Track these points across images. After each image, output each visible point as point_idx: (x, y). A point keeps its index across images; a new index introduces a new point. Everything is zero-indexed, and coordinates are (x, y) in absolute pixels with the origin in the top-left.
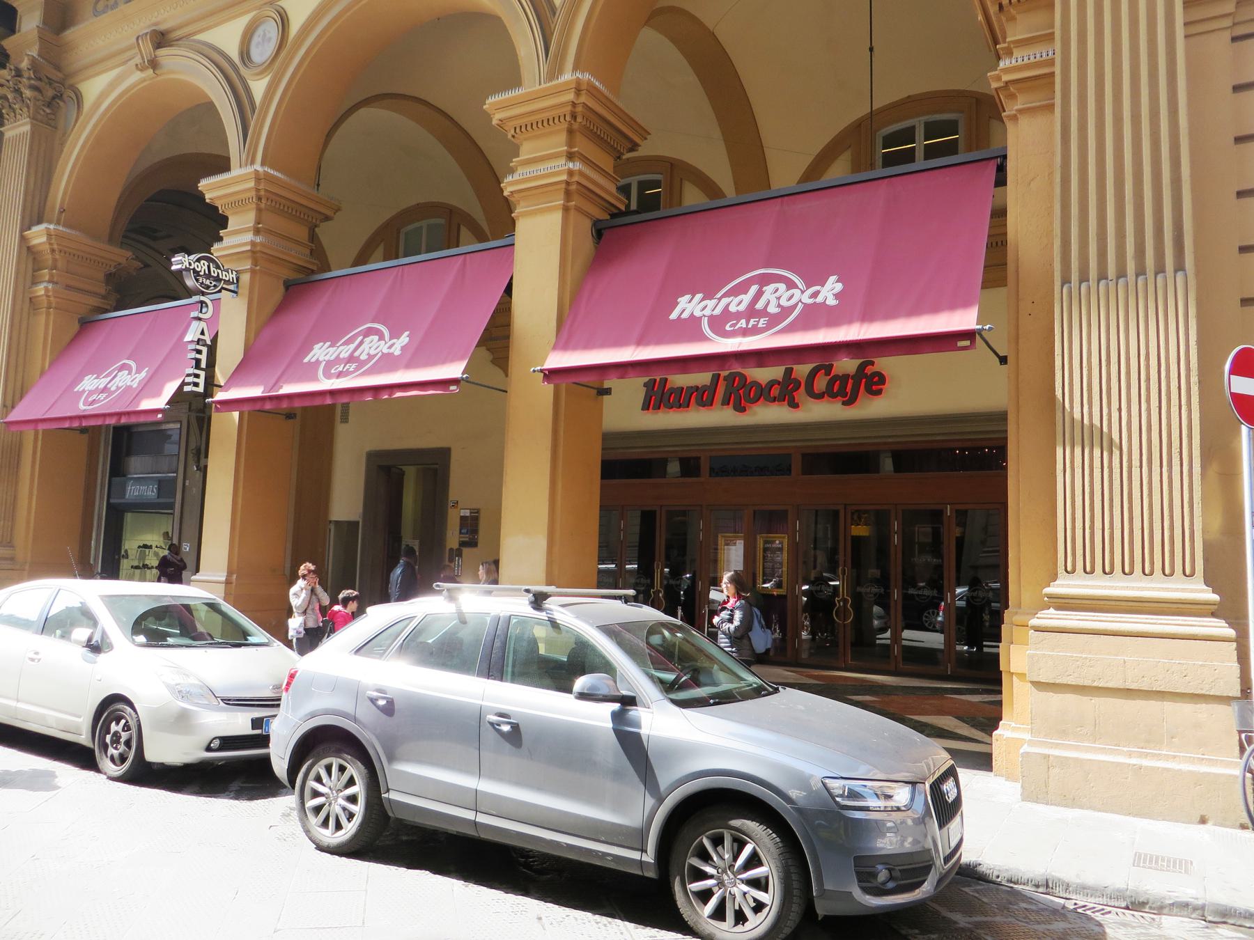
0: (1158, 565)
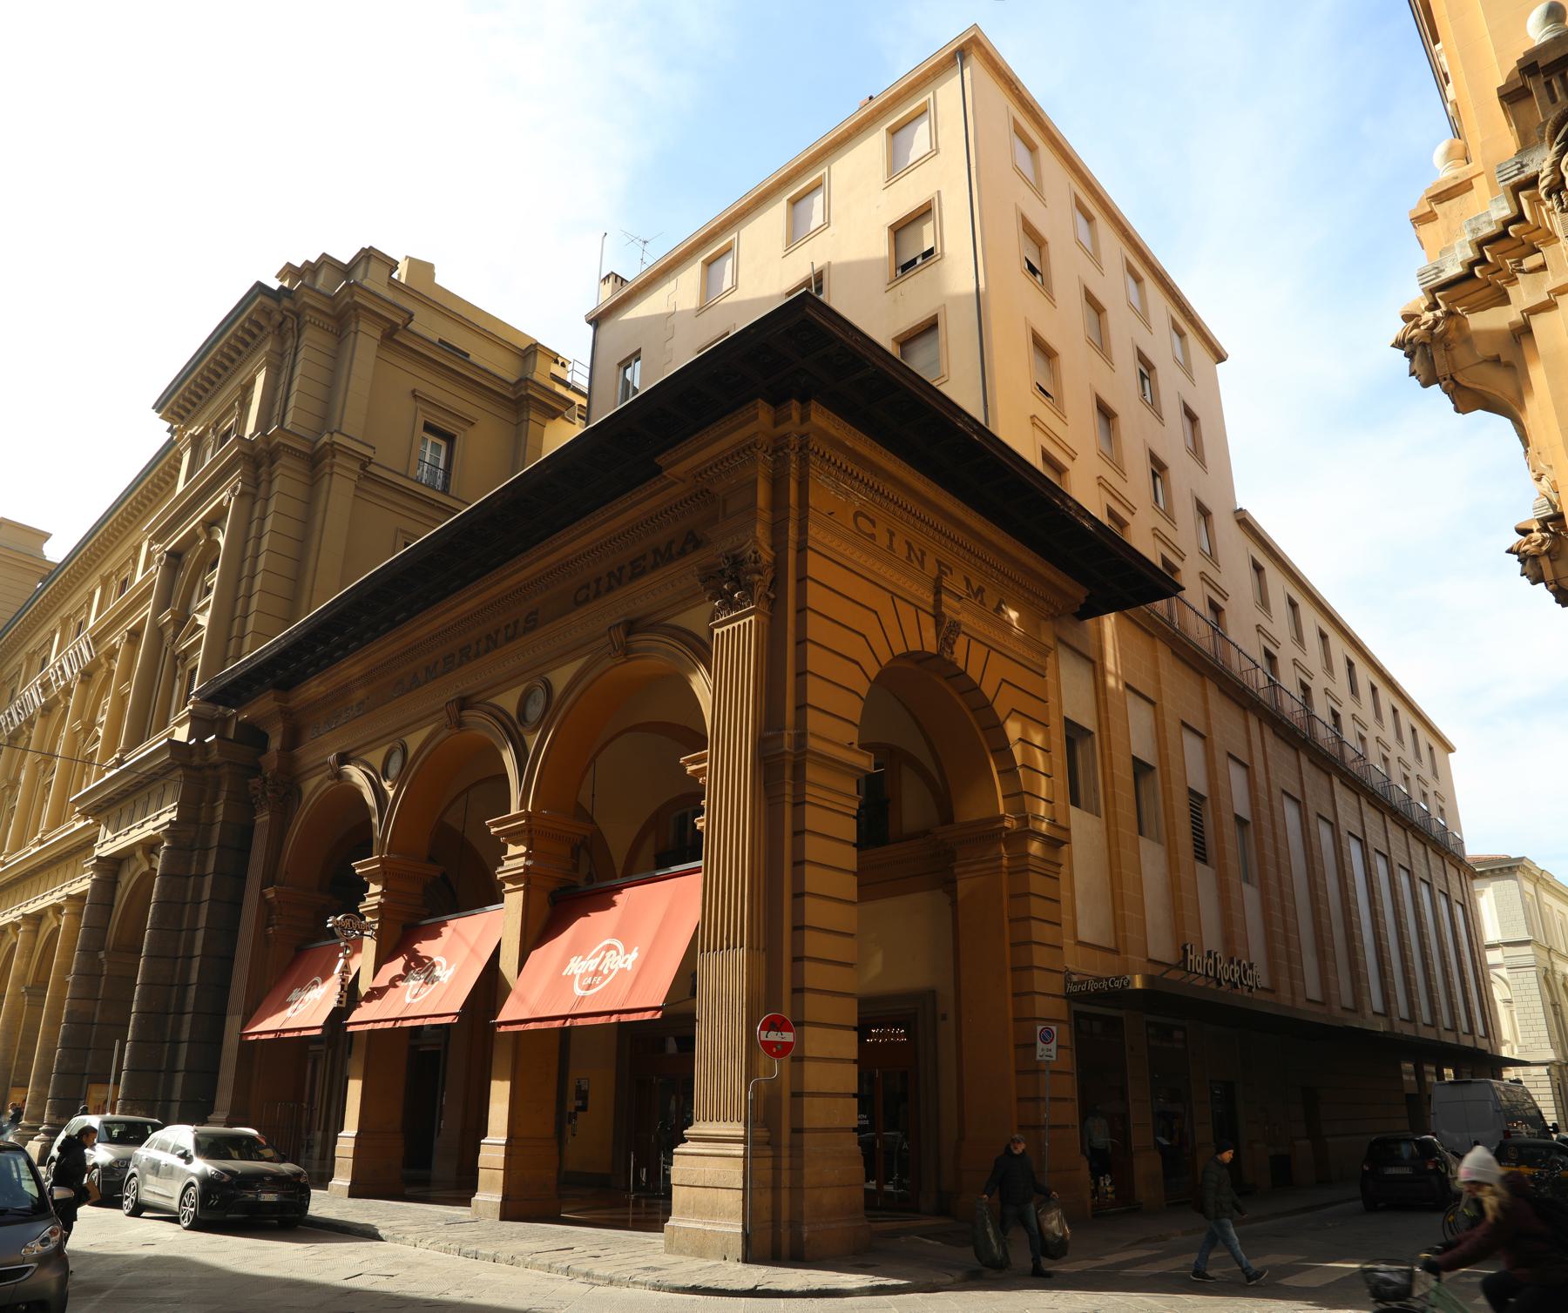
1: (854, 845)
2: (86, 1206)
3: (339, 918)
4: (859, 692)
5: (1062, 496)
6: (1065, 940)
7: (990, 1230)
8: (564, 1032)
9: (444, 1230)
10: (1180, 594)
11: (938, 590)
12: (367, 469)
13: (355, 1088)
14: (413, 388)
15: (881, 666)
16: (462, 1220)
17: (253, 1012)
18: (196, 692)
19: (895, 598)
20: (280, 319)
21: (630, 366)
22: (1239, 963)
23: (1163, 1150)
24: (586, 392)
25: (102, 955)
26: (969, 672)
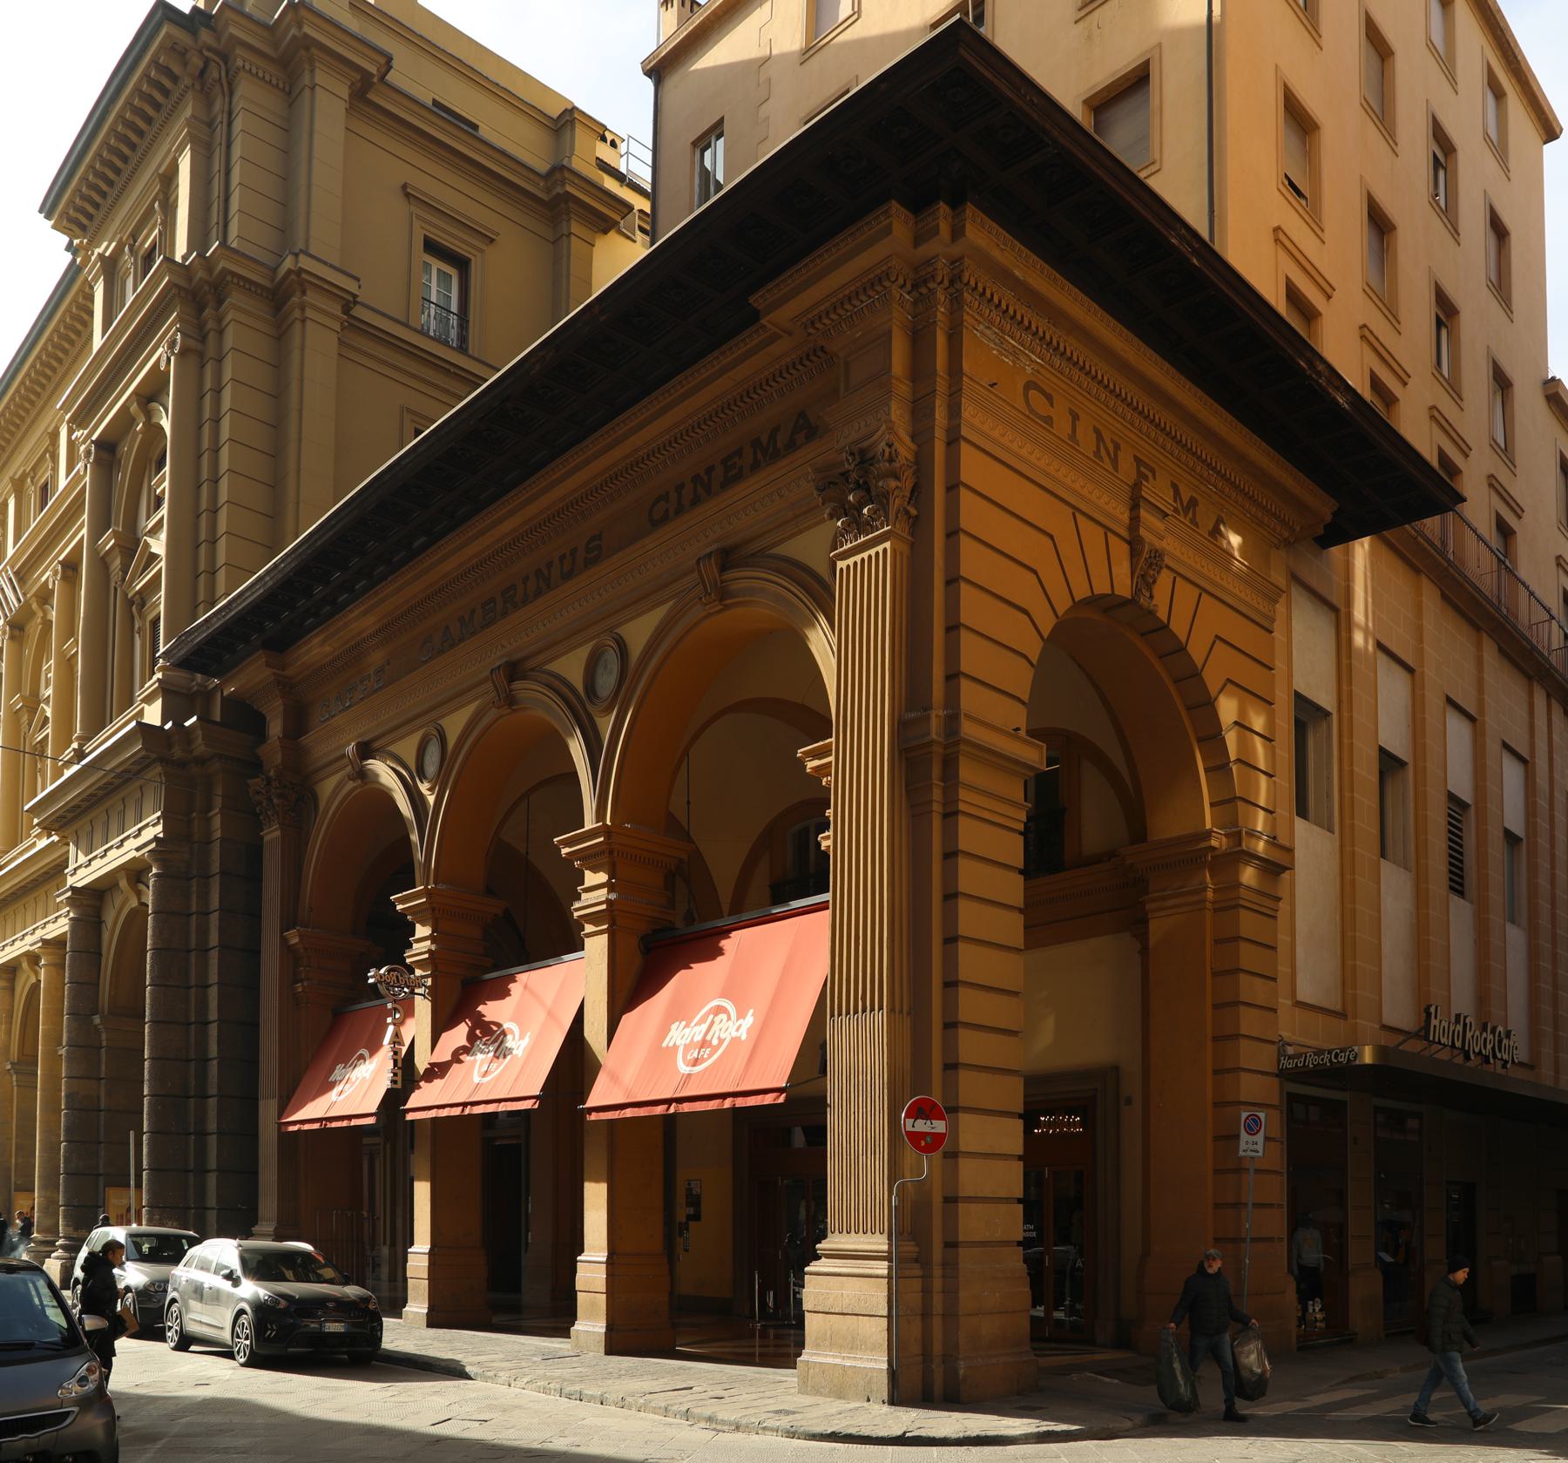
0: (853, 1229)
1: (1021, 872)
2: (124, 1338)
3: (382, 971)
4: (1029, 610)
5: (1309, 354)
6: (1280, 1000)
7: (1177, 1365)
8: (669, 1120)
9: (541, 1367)
10: (1458, 507)
11: (1135, 503)
12: (351, 313)
13: (422, 1192)
14: (403, 182)
15: (1057, 617)
16: (561, 1354)
17: (290, 1096)
18: (163, 653)
19: (1077, 514)
20: (201, 64)
21: (708, 146)
22: (1493, 1030)
23: (1385, 1268)
24: (648, 188)
25: (97, 1020)
26: (1173, 627)
